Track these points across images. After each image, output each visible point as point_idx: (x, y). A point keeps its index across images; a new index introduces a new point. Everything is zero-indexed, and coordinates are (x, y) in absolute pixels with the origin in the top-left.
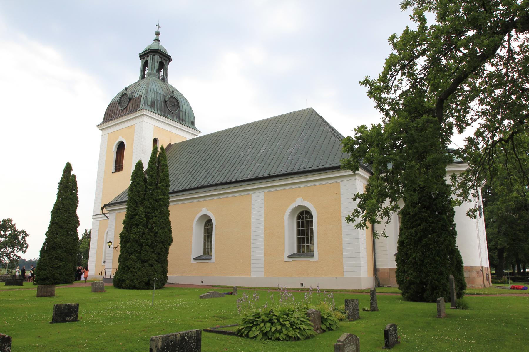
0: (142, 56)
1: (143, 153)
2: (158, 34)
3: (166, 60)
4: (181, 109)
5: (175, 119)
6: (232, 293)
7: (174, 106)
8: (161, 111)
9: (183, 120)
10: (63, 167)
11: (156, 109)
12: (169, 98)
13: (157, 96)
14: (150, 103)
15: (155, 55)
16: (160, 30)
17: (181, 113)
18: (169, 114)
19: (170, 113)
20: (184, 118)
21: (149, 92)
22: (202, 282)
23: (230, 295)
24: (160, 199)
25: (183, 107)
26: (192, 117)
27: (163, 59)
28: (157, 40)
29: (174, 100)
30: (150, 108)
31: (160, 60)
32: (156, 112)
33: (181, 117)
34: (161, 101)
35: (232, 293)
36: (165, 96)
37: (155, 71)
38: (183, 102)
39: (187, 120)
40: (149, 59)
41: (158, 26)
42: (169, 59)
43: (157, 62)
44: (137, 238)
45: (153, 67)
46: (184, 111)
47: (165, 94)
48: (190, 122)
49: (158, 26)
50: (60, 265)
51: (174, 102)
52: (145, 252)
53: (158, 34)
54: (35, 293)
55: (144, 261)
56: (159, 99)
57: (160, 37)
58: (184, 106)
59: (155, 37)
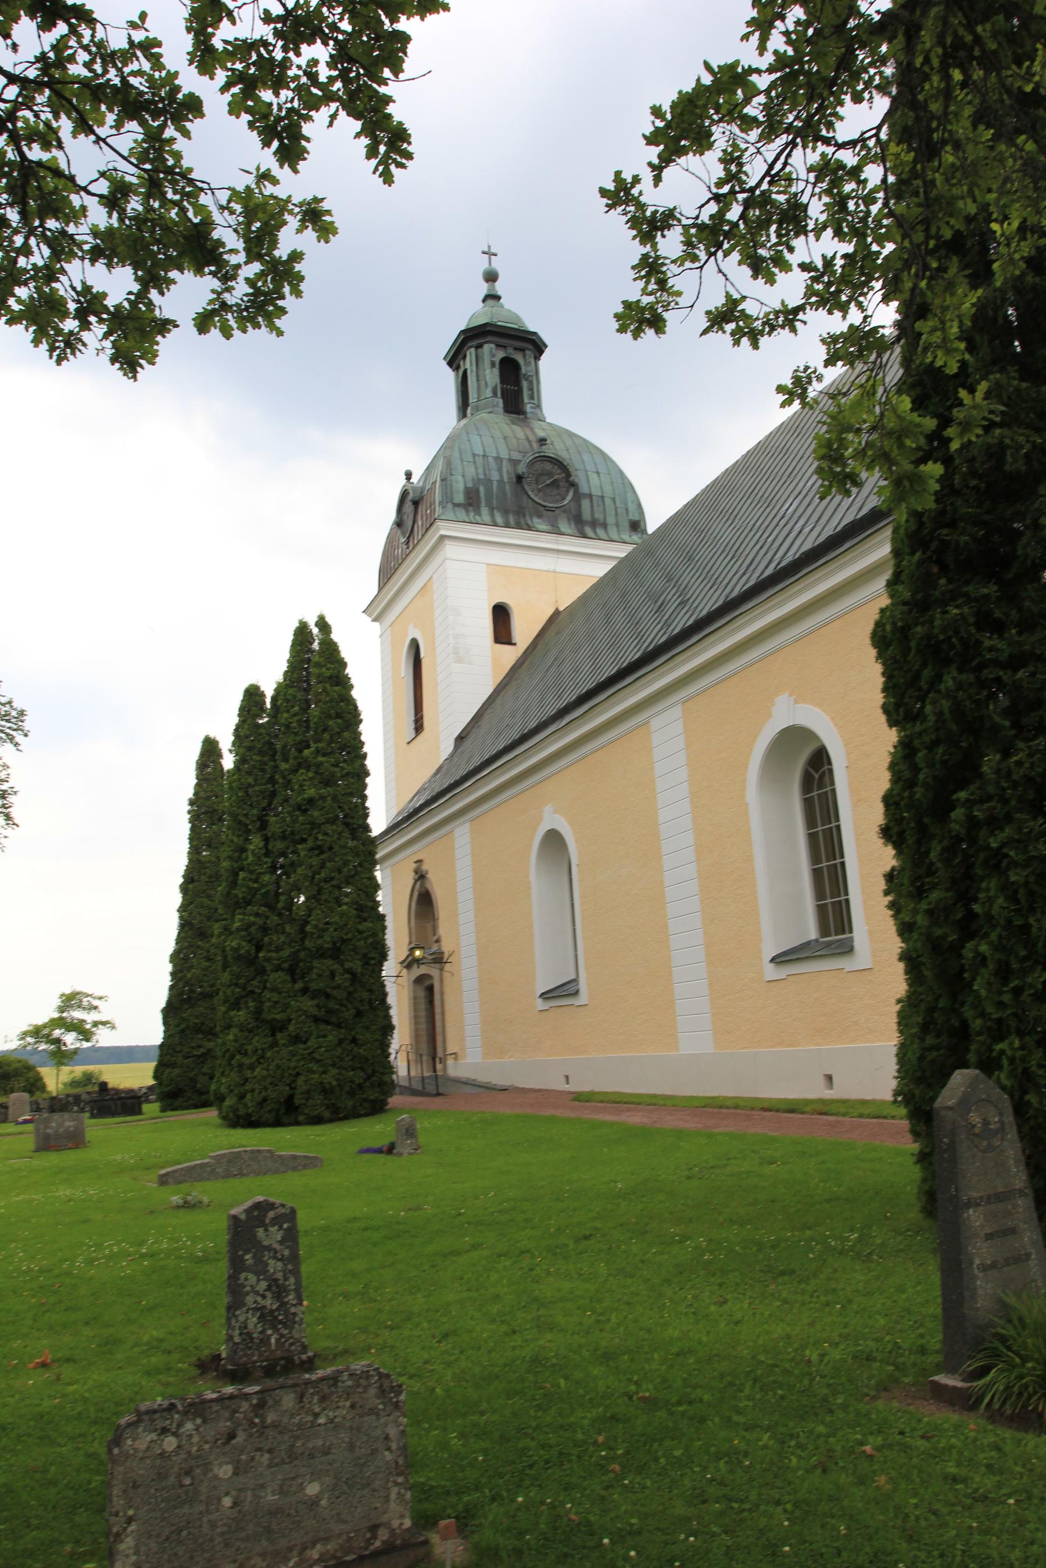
0: (454, 359)
1: (460, 661)
2: (491, 277)
3: (522, 350)
4: (584, 489)
5: (564, 526)
6: (390, 1149)
7: (555, 484)
8: (505, 512)
9: (594, 524)
10: (195, 751)
11: (485, 510)
12: (531, 464)
13: (486, 467)
14: (460, 498)
15: (479, 347)
16: (497, 264)
17: (585, 504)
18: (540, 516)
19: (541, 511)
20: (599, 516)
21: (456, 462)
22: (829, 1078)
23: (381, 1158)
24: (311, 801)
25: (591, 482)
26: (632, 507)
27: (510, 351)
28: (492, 297)
29: (548, 466)
30: (461, 514)
31: (501, 354)
32: (487, 518)
33: (586, 515)
34: (501, 482)
35: (390, 1149)
36: (514, 463)
37: (488, 393)
38: (590, 467)
39: (611, 520)
40: (468, 363)
41: (489, 254)
42: (536, 346)
43: (493, 365)
44: (246, 947)
45: (482, 383)
46: (596, 492)
47: (516, 456)
48: (626, 524)
49: (489, 254)
50: (209, 1050)
51: (550, 474)
52: (275, 997)
53: (491, 277)
54: (29, 1142)
55: (276, 1028)
56: (495, 476)
57: (500, 287)
58: (594, 477)
59: (484, 288)
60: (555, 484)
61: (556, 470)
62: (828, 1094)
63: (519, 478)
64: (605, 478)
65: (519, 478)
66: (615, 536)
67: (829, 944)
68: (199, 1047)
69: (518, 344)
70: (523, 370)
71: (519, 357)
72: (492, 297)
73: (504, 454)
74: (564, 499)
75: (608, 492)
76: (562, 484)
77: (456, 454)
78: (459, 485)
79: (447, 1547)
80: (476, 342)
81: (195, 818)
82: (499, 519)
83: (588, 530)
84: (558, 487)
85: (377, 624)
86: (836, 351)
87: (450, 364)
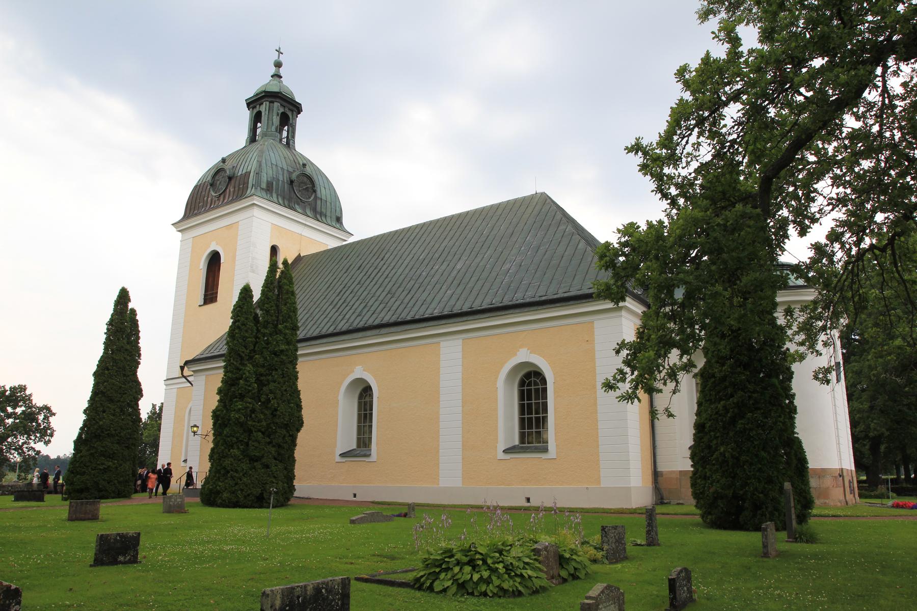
1: (253, 272)
2: (278, 65)
3: (292, 111)
4: (319, 195)
6: (405, 515)
8: (284, 199)
9: (321, 214)
11: (274, 195)
12: (298, 177)
13: (277, 172)
14: (264, 186)
15: (273, 102)
16: (282, 59)
17: (319, 202)
18: (298, 204)
19: (300, 202)
20: (323, 210)
23: (403, 518)
24: (282, 351)
25: (322, 192)
28: (277, 76)
29: (305, 179)
31: (282, 110)
32: (275, 200)
33: (318, 209)
34: (283, 181)
35: (405, 515)
36: (290, 173)
37: (273, 129)
39: (328, 214)
40: (264, 108)
41: (279, 51)
46: (324, 198)
47: (291, 170)
48: (334, 218)
49: (279, 51)
51: (305, 184)
52: (256, 444)
53: (278, 65)
55: (253, 460)
56: (281, 179)
58: (323, 189)
59: (273, 70)
62: (529, 504)
63: (292, 182)
64: (328, 191)
65: (292, 182)
66: (329, 222)
67: (522, 447)
68: (103, 464)
69: (291, 107)
71: (290, 114)
73: (285, 167)
75: (329, 200)
77: (264, 161)
78: (264, 179)
80: (270, 99)
81: (109, 333)
82: (281, 202)
83: (318, 216)
85: (180, 234)
87: (249, 105)
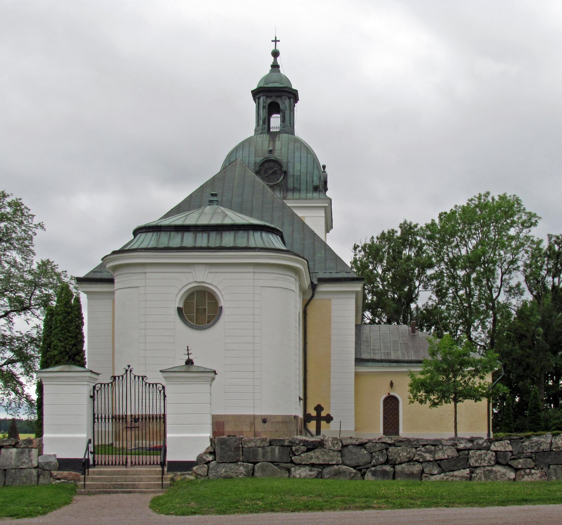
2: (276, 54)
3: (280, 97)
7: (275, 173)
16: (280, 47)
20: (297, 186)
28: (275, 66)
31: (269, 101)
41: (276, 41)
43: (264, 107)
48: (311, 188)
51: (272, 168)
53: (276, 54)
60: (275, 173)
61: (271, 164)
69: (276, 94)
70: (281, 107)
72: (275, 66)
74: (278, 179)
76: (278, 172)
79: (1, 204)
84: (276, 174)
86: (9, 229)
